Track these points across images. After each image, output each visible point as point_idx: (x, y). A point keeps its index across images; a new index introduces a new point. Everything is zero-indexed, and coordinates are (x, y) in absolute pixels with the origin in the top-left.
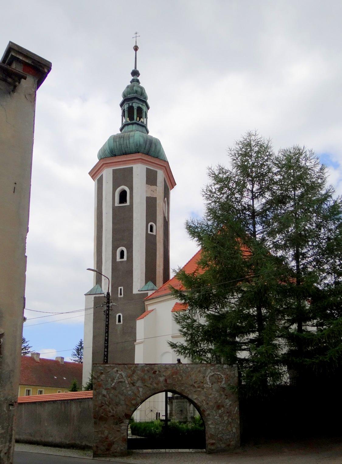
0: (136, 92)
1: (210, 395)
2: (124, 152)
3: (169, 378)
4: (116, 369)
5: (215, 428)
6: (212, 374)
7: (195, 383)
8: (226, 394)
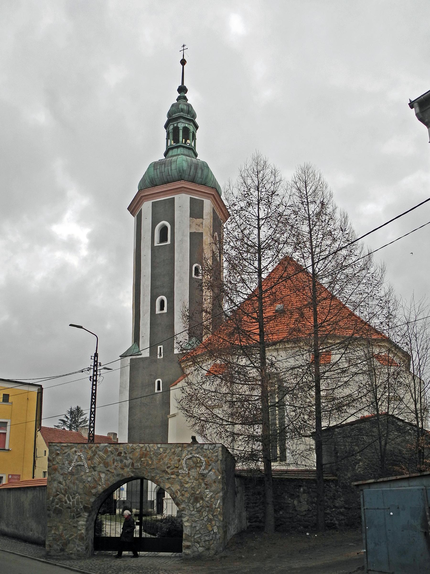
0: (182, 110)
1: (186, 484)
2: (166, 180)
3: (137, 462)
4: (74, 449)
5: (191, 526)
6: (189, 457)
7: (168, 468)
8: (206, 483)
